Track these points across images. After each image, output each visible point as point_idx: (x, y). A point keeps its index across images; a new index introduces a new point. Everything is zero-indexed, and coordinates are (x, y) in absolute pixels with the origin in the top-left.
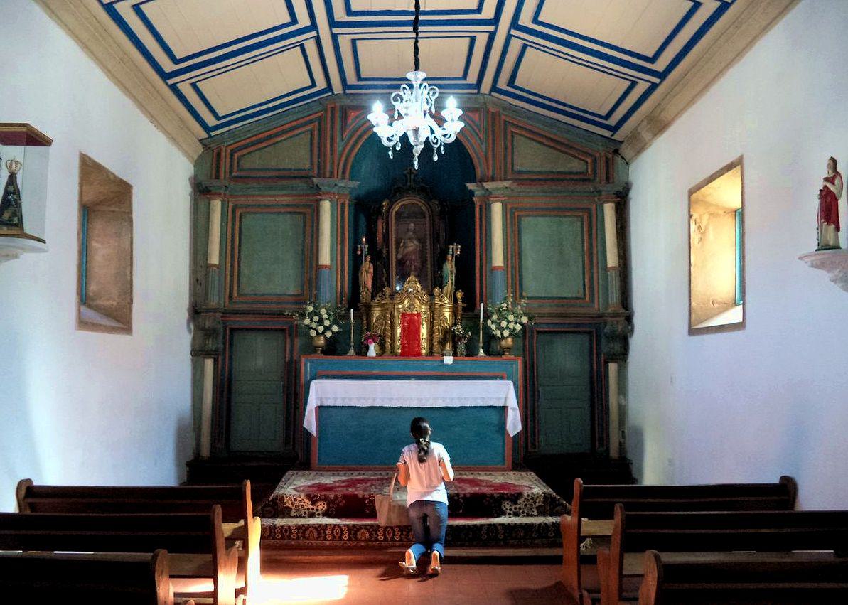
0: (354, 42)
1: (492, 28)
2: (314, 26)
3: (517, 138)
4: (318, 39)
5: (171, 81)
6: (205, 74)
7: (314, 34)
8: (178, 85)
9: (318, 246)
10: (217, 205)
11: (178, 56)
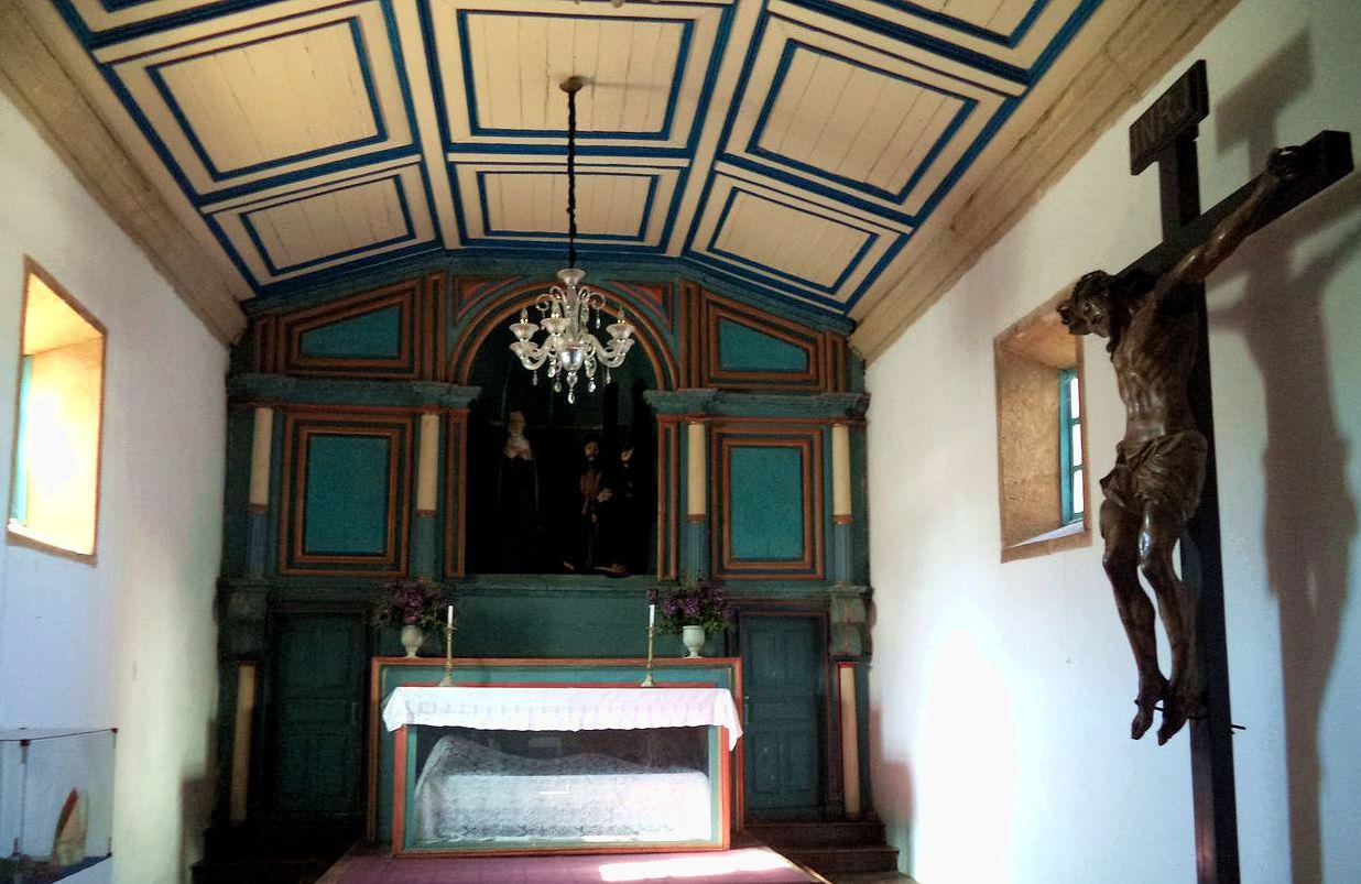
0: (480, 176)
1: (684, 162)
2: (416, 147)
3: (723, 324)
4: (423, 166)
5: (206, 209)
6: (376, 172)
7: (416, 158)
8: (458, 166)
9: (1089, 15)
10: (264, 418)
11: (484, 124)
